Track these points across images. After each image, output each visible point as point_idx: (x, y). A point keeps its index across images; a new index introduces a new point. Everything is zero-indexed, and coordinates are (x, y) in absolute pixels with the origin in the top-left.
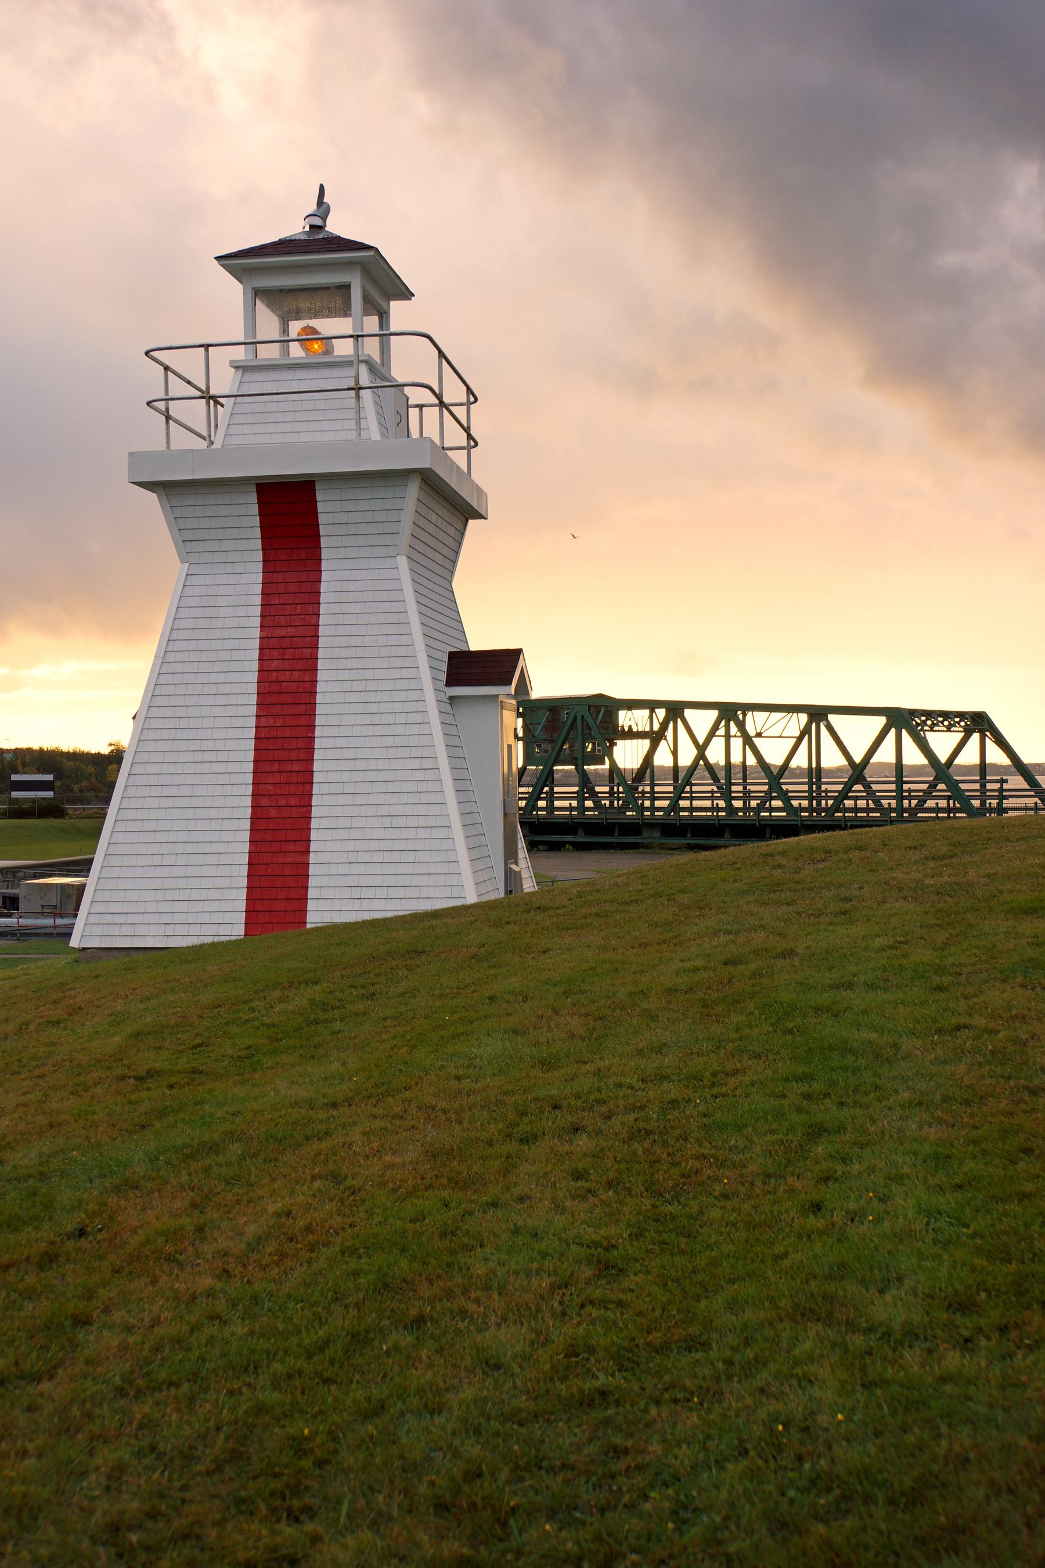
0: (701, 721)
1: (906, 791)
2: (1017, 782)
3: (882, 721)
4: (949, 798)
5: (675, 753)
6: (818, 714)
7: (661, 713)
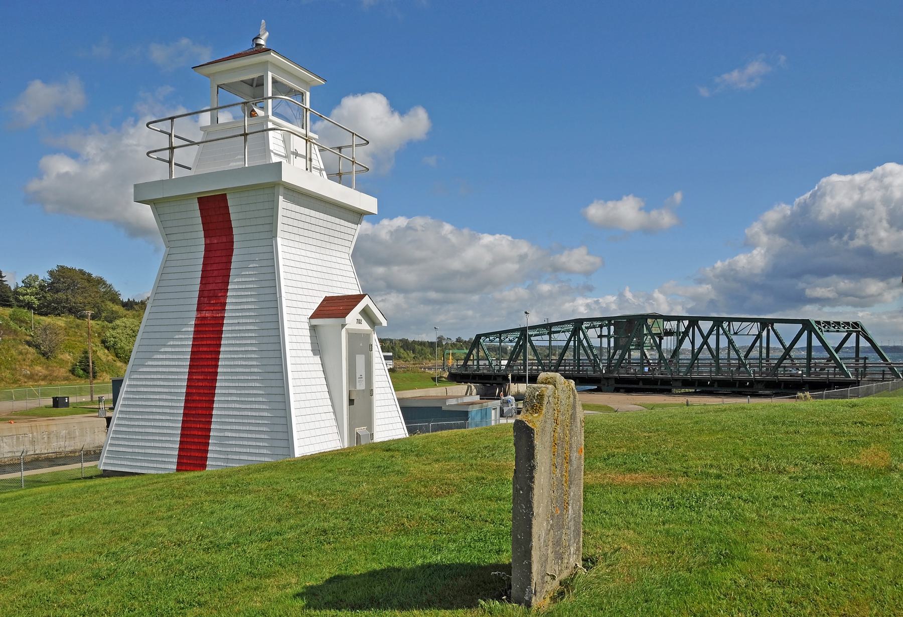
0: (706, 326)
1: (862, 358)
2: (873, 357)
3: (800, 326)
4: (835, 367)
5: (693, 343)
6: (765, 324)
7: (686, 323)
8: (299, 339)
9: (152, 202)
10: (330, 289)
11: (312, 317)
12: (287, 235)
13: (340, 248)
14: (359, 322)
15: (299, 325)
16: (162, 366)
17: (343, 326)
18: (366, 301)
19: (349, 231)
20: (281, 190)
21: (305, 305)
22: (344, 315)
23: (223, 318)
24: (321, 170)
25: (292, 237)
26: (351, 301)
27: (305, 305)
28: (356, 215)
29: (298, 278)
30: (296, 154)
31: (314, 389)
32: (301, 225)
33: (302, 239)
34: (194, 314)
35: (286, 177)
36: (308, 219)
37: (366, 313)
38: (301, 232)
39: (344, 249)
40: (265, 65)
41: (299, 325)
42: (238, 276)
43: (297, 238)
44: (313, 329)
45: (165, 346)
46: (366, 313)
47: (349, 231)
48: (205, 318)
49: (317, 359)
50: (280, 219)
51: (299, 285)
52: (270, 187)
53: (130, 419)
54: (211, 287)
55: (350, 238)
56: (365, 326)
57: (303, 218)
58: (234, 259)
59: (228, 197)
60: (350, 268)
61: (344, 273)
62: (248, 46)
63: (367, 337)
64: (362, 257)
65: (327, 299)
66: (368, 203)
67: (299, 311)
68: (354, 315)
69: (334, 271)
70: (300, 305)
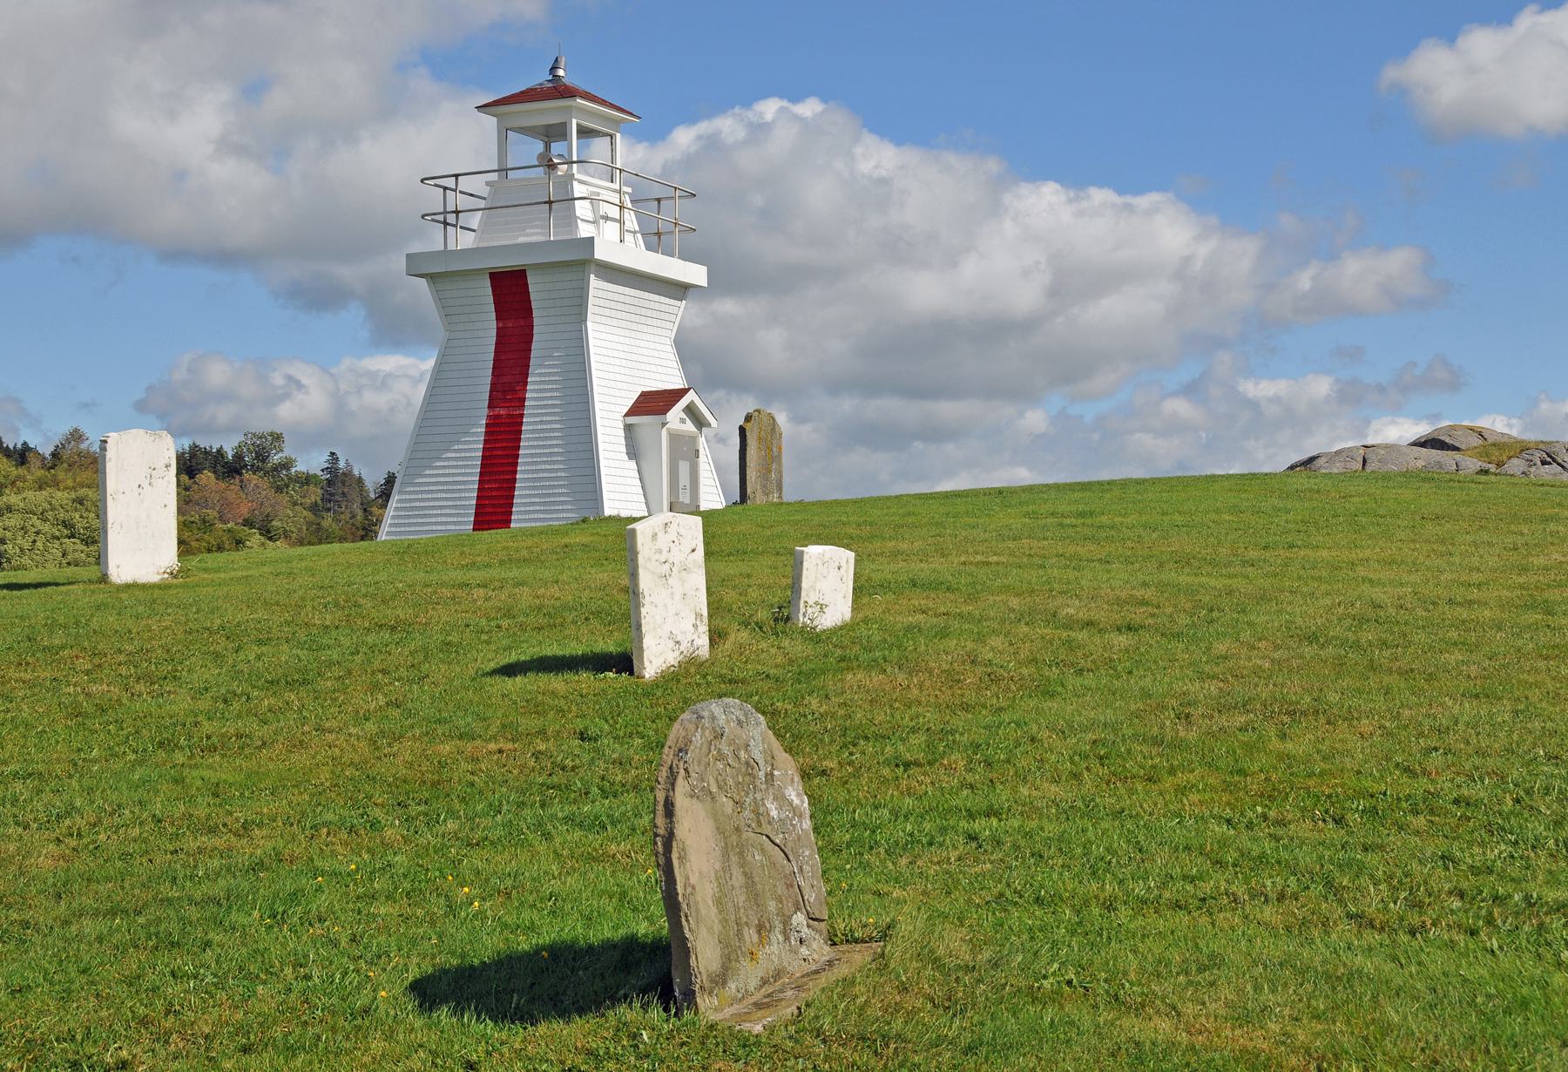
8: (613, 439)
9: (432, 277)
10: (647, 382)
11: (628, 414)
12: (598, 318)
13: (659, 331)
14: (683, 421)
15: (612, 423)
16: (454, 475)
17: (664, 424)
18: (691, 397)
19: (671, 309)
20: (593, 267)
21: (619, 401)
22: (664, 411)
23: (522, 415)
24: (635, 233)
25: (604, 320)
26: (674, 396)
27: (619, 401)
28: (678, 290)
29: (611, 368)
30: (606, 218)
31: (629, 497)
32: (613, 305)
33: (615, 322)
34: (485, 411)
35: (600, 253)
36: (622, 298)
37: (691, 411)
38: (614, 313)
39: (664, 332)
40: (569, 111)
41: (612, 423)
42: (542, 366)
43: (609, 321)
44: (628, 428)
45: (448, 450)
46: (691, 411)
47: (671, 309)
48: (498, 416)
49: (633, 464)
50: (591, 300)
51: (612, 376)
52: (580, 262)
53: (546, 438)
54: (505, 379)
55: (672, 318)
56: (690, 427)
57: (616, 297)
58: (534, 346)
59: (530, 280)
60: (672, 357)
61: (665, 363)
62: (540, 78)
63: (693, 440)
64: (684, 347)
65: (644, 394)
66: (696, 274)
67: (613, 408)
68: (676, 414)
69: (643, 366)
70: (613, 400)
